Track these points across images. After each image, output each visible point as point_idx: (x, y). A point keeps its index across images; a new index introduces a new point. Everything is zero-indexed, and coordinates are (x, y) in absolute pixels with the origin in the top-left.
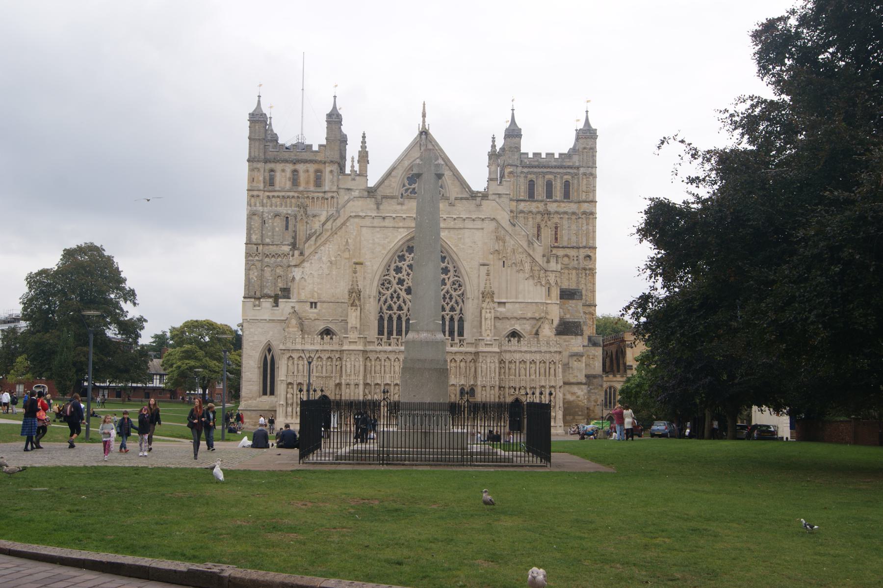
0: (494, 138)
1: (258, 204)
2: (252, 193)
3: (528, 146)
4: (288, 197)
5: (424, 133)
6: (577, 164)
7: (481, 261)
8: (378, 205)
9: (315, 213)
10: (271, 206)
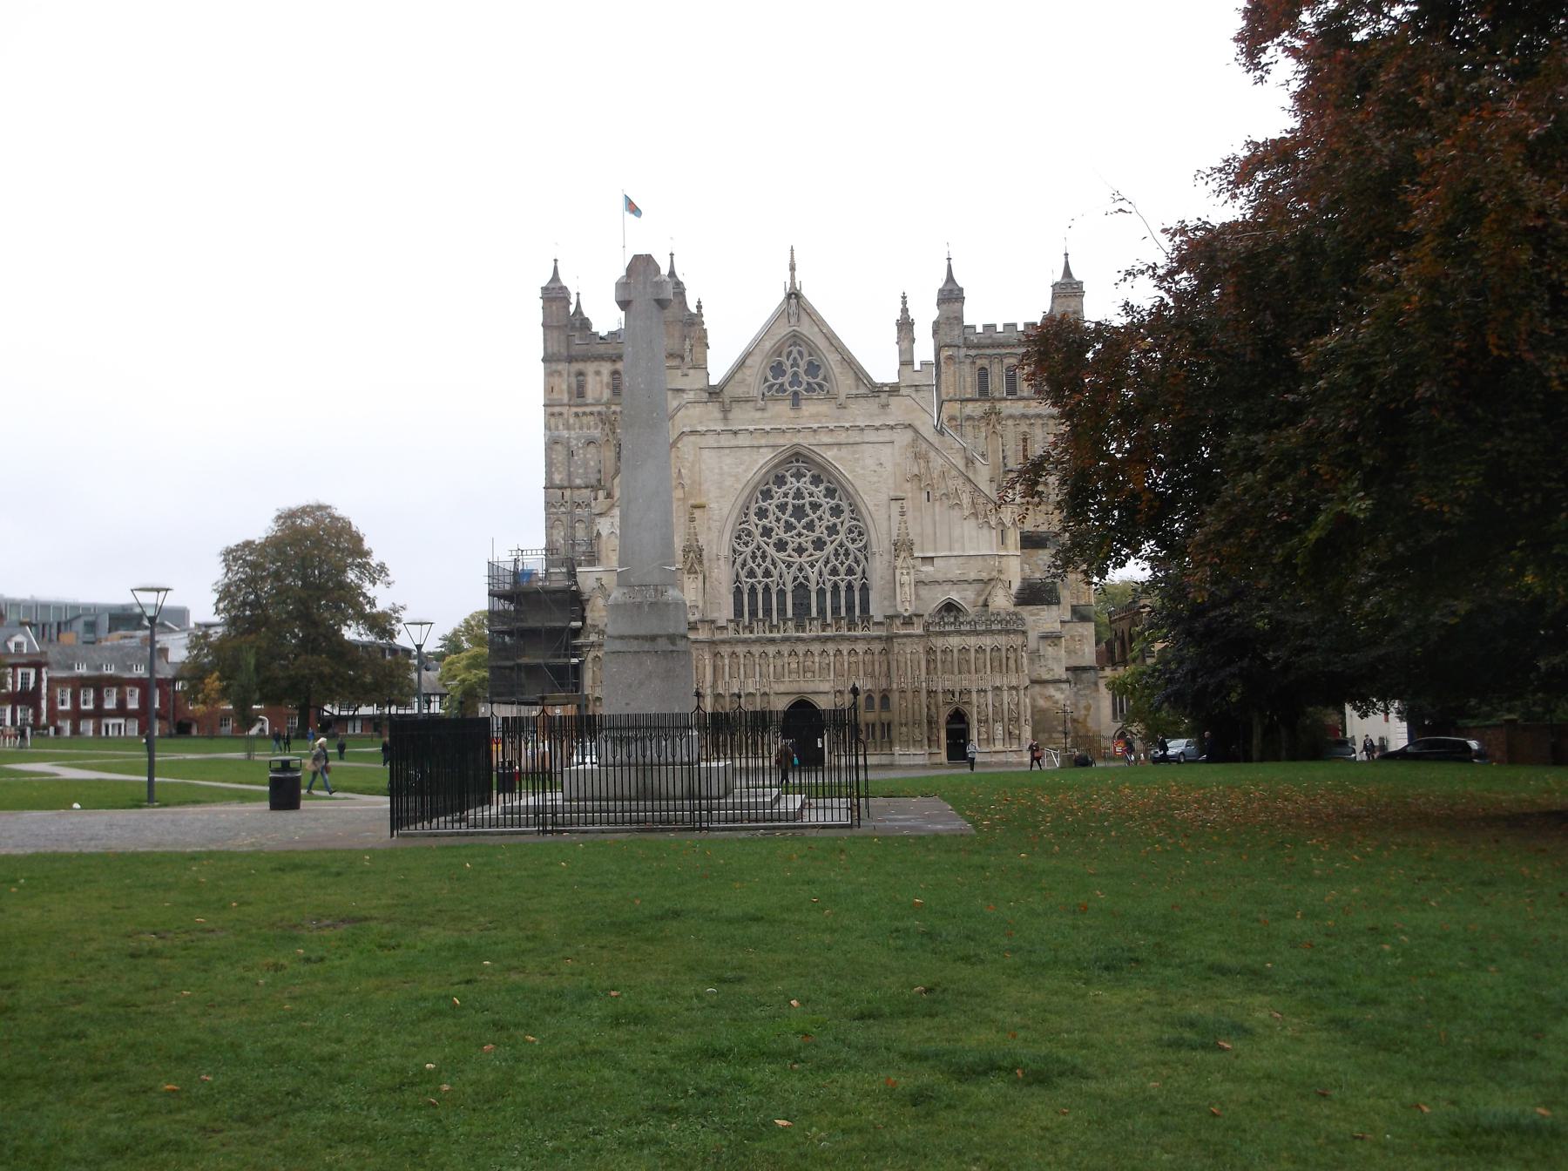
2: (550, 410)
3: (976, 315)
5: (794, 295)
7: (893, 494)
8: (725, 411)
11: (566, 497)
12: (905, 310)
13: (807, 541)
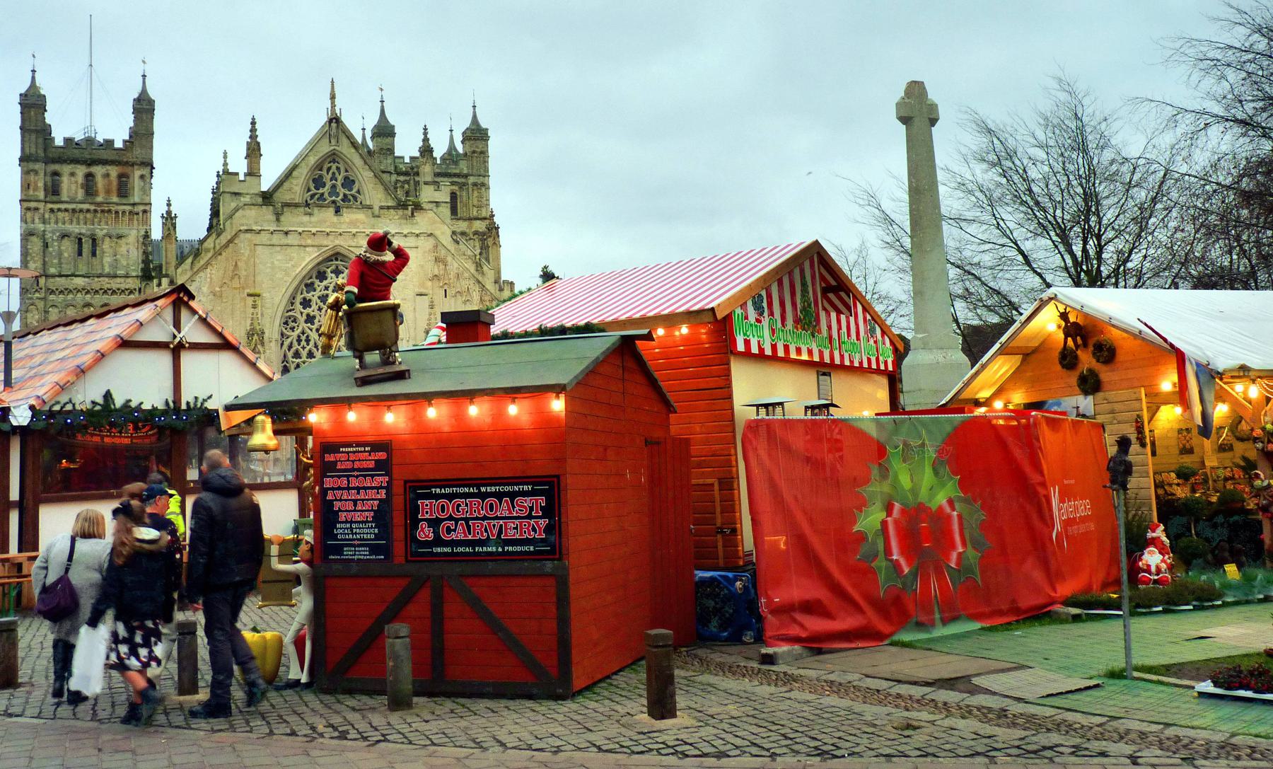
0: (425, 129)
1: (37, 220)
2: (26, 205)
4: (81, 211)
5: (335, 120)
6: (465, 172)
8: (278, 216)
9: (120, 232)
10: (57, 222)
11: (571, 280)
12: (426, 140)
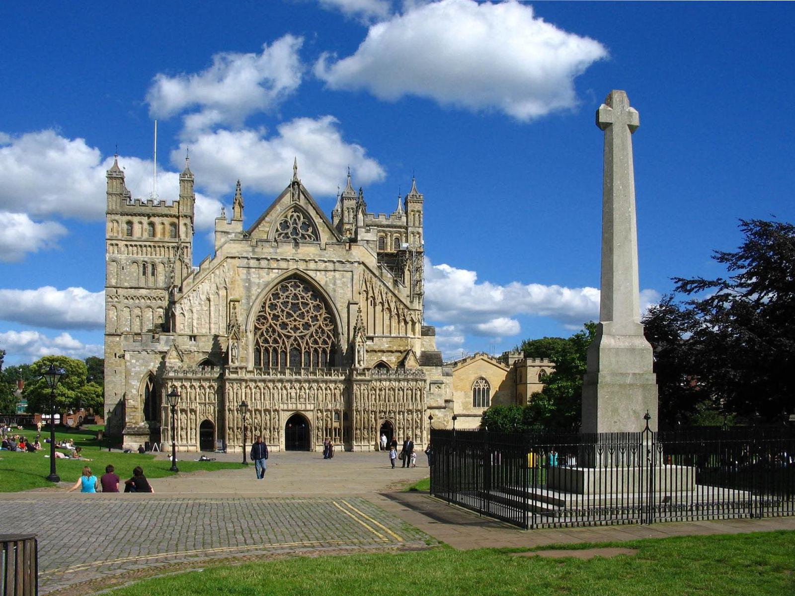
13: (300, 324)
